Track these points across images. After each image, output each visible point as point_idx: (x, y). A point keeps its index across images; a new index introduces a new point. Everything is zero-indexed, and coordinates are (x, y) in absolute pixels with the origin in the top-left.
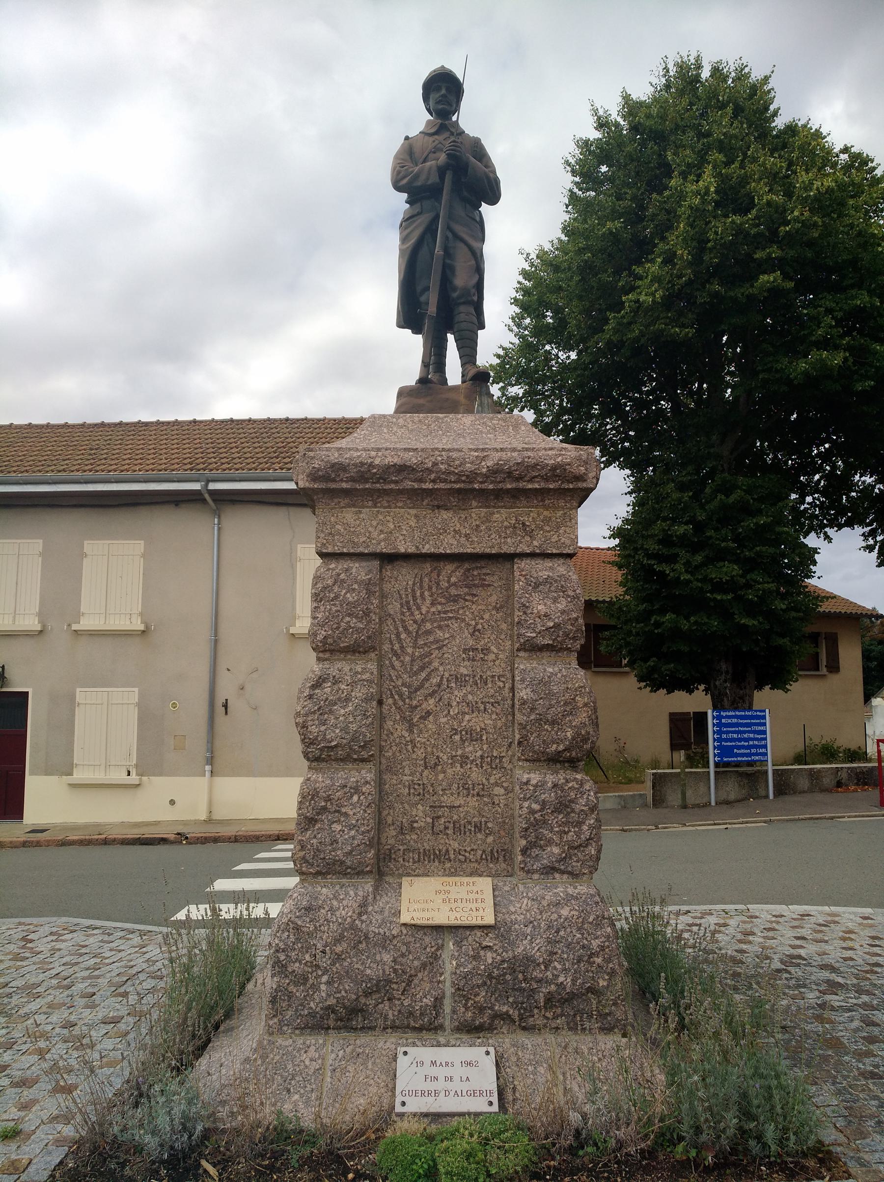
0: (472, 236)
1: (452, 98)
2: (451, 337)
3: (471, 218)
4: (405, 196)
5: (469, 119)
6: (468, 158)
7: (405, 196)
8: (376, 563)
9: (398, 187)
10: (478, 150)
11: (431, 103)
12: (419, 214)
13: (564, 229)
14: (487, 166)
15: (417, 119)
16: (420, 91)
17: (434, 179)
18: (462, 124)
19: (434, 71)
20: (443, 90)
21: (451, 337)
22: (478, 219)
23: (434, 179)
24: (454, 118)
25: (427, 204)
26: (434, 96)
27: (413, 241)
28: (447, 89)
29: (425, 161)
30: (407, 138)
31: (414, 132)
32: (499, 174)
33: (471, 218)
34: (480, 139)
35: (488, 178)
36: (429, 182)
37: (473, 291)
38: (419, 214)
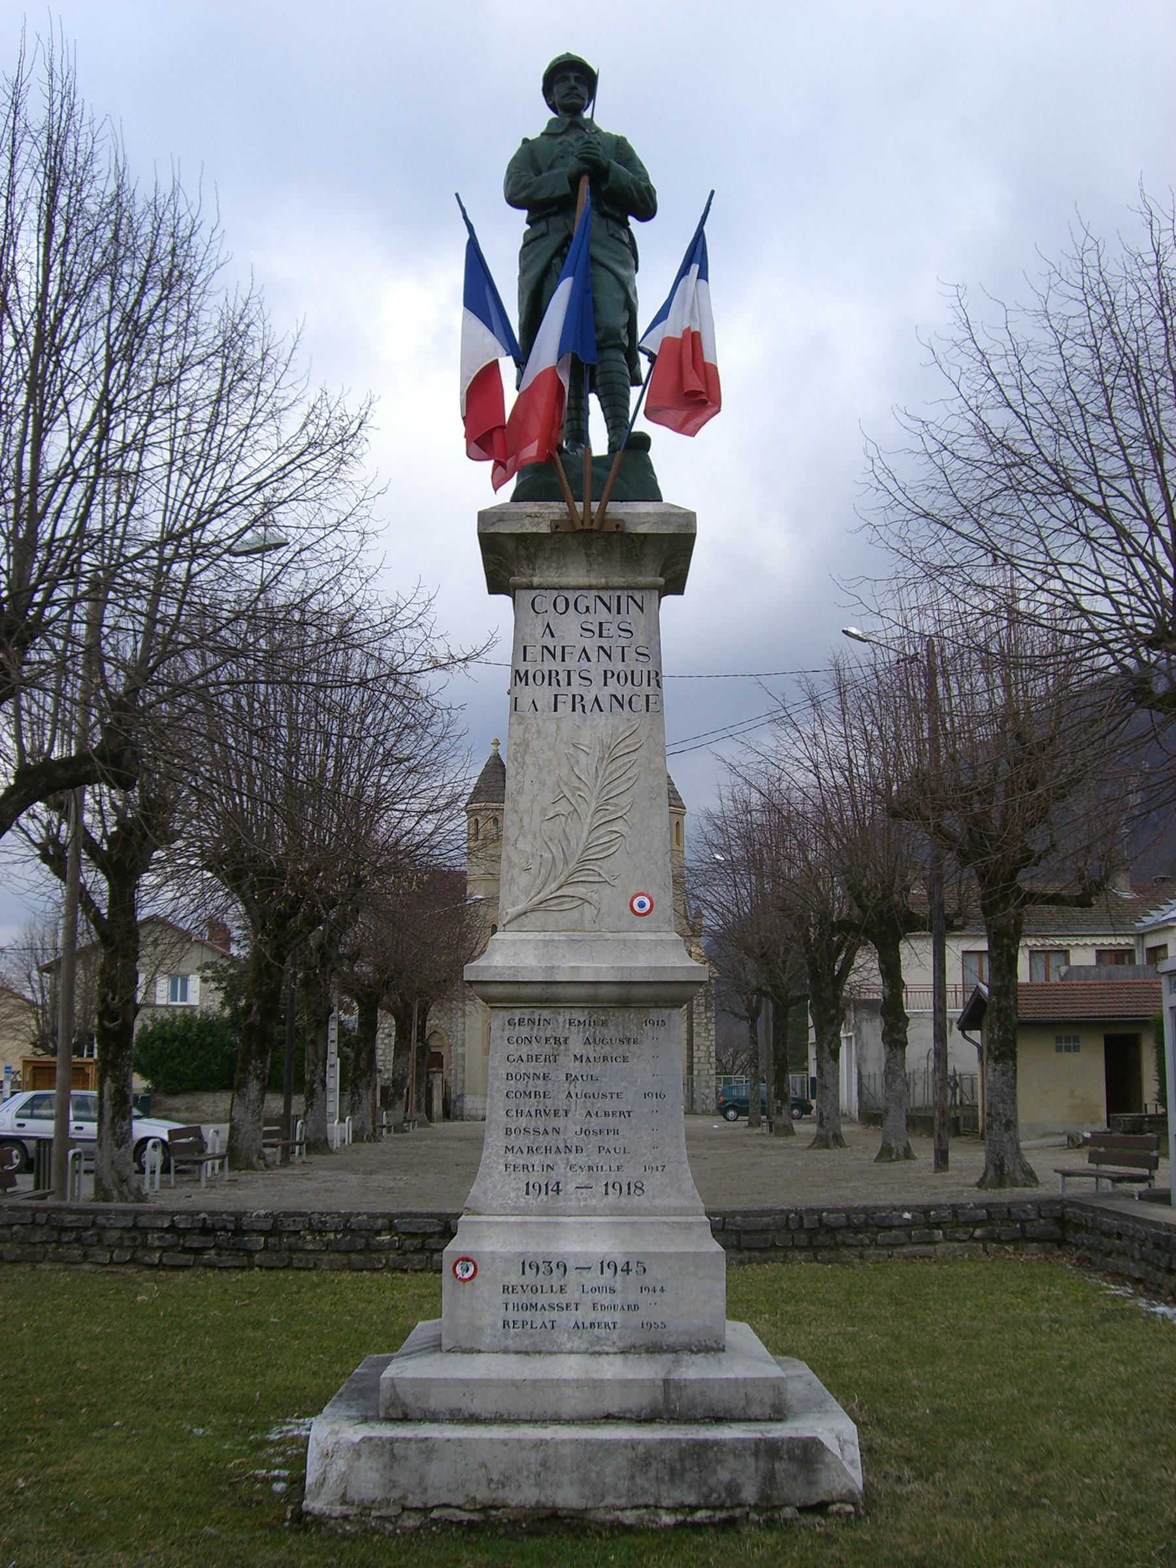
0: (618, 262)
1: (583, 90)
2: (594, 401)
3: (617, 239)
4: (524, 214)
5: (607, 114)
6: (609, 164)
7: (524, 214)
8: (441, 653)
9: (514, 201)
10: (621, 148)
11: (556, 98)
12: (543, 235)
13: (528, 222)
14: (635, 172)
15: (537, 118)
16: (540, 84)
17: (566, 189)
18: (598, 122)
19: (559, 59)
20: (570, 82)
21: (594, 401)
22: (626, 240)
23: (566, 189)
24: (587, 115)
25: (557, 222)
26: (559, 90)
27: (535, 271)
28: (577, 79)
29: (551, 167)
30: (525, 141)
31: (534, 134)
32: (654, 181)
33: (617, 239)
34: (624, 139)
35: (637, 186)
36: (555, 195)
37: (623, 332)
38: (543, 235)
